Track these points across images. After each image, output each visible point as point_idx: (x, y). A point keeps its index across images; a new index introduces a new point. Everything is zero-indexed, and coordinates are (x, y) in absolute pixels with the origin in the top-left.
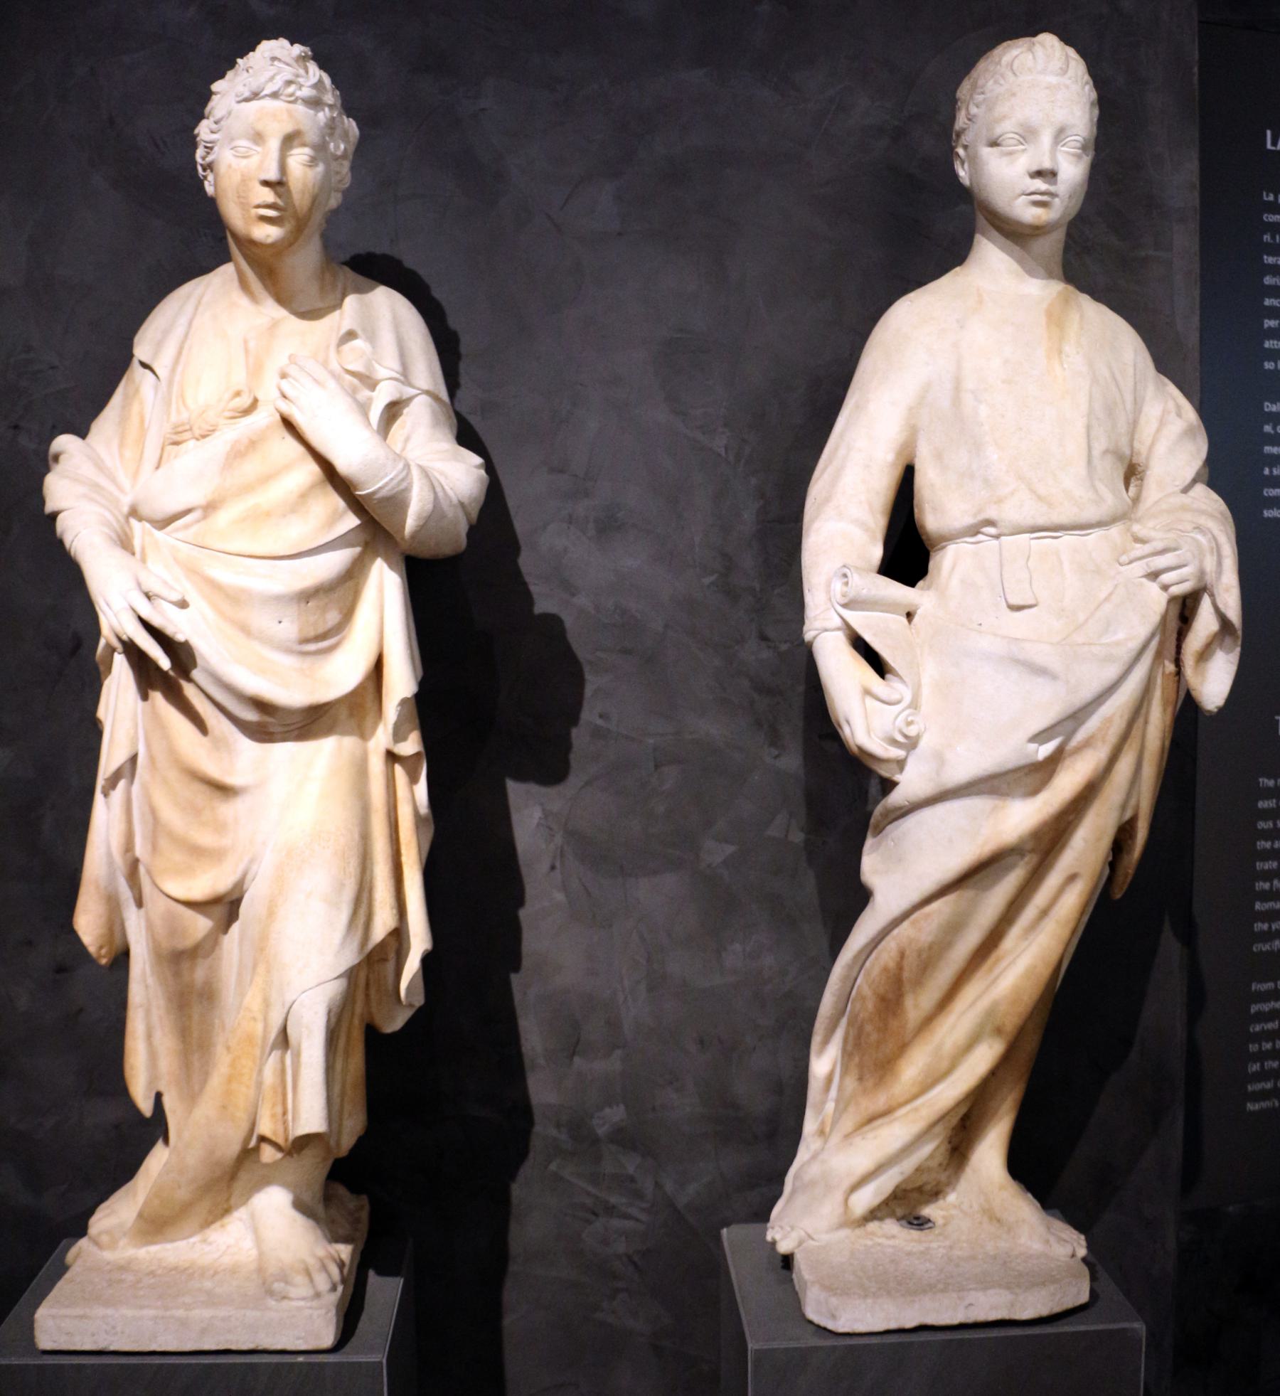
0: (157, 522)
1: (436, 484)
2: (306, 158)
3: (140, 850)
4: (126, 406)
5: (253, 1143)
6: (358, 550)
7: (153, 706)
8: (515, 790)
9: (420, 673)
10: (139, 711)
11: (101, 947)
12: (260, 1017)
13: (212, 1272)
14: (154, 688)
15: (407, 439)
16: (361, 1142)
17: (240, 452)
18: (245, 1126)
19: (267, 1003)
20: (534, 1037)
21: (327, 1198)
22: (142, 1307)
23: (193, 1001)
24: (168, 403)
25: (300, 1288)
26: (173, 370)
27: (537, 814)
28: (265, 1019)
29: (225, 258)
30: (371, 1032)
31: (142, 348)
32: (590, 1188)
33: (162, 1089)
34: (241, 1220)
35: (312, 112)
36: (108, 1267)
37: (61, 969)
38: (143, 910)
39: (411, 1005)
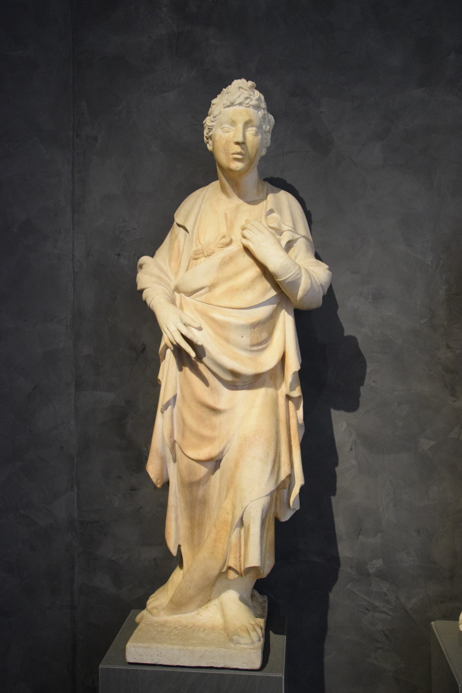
0: (188, 293)
1: (312, 276)
2: (254, 132)
3: (176, 437)
4: (171, 244)
5: (224, 570)
6: (275, 306)
7: (185, 374)
8: (334, 413)
10: (178, 376)
11: (158, 480)
12: (230, 513)
16: (273, 570)
17: (225, 263)
18: (221, 562)
19: (234, 506)
20: (341, 525)
21: (252, 596)
22: (174, 644)
23: (197, 506)
26: (194, 227)
27: (345, 425)
28: (233, 513)
29: (216, 178)
30: (277, 520)
31: (179, 218)
32: (366, 598)
34: (215, 605)
35: (256, 111)
36: (157, 624)
37: (133, 489)
38: (176, 463)
39: (294, 509)
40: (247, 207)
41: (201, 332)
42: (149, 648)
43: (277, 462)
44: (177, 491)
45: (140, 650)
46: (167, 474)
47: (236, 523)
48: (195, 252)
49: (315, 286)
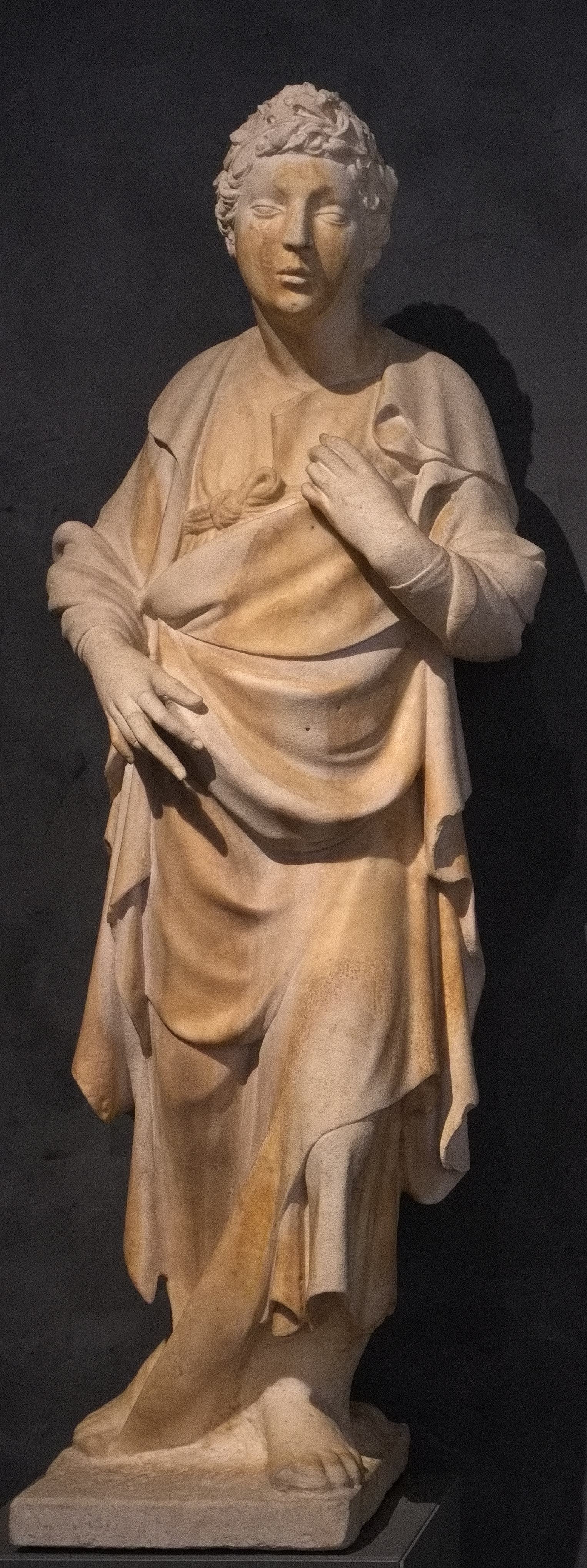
0: (173, 619)
3: (149, 987)
6: (397, 650)
7: (168, 823)
9: (468, 790)
11: (102, 1099)
12: (277, 1167)
13: (217, 1473)
14: (168, 804)
15: (455, 528)
17: (261, 545)
18: (256, 1294)
19: (284, 1150)
21: (355, 1415)
22: (132, 1498)
23: (206, 1167)
24: (186, 488)
25: (310, 1477)
28: (282, 1167)
29: (251, 322)
31: (157, 428)
33: (168, 1273)
34: (250, 1421)
35: (341, 165)
38: (152, 1059)
39: (453, 1171)
40: (328, 398)
41: (202, 716)
42: (68, 1507)
46: (130, 1090)
48: (194, 515)
49: (491, 602)
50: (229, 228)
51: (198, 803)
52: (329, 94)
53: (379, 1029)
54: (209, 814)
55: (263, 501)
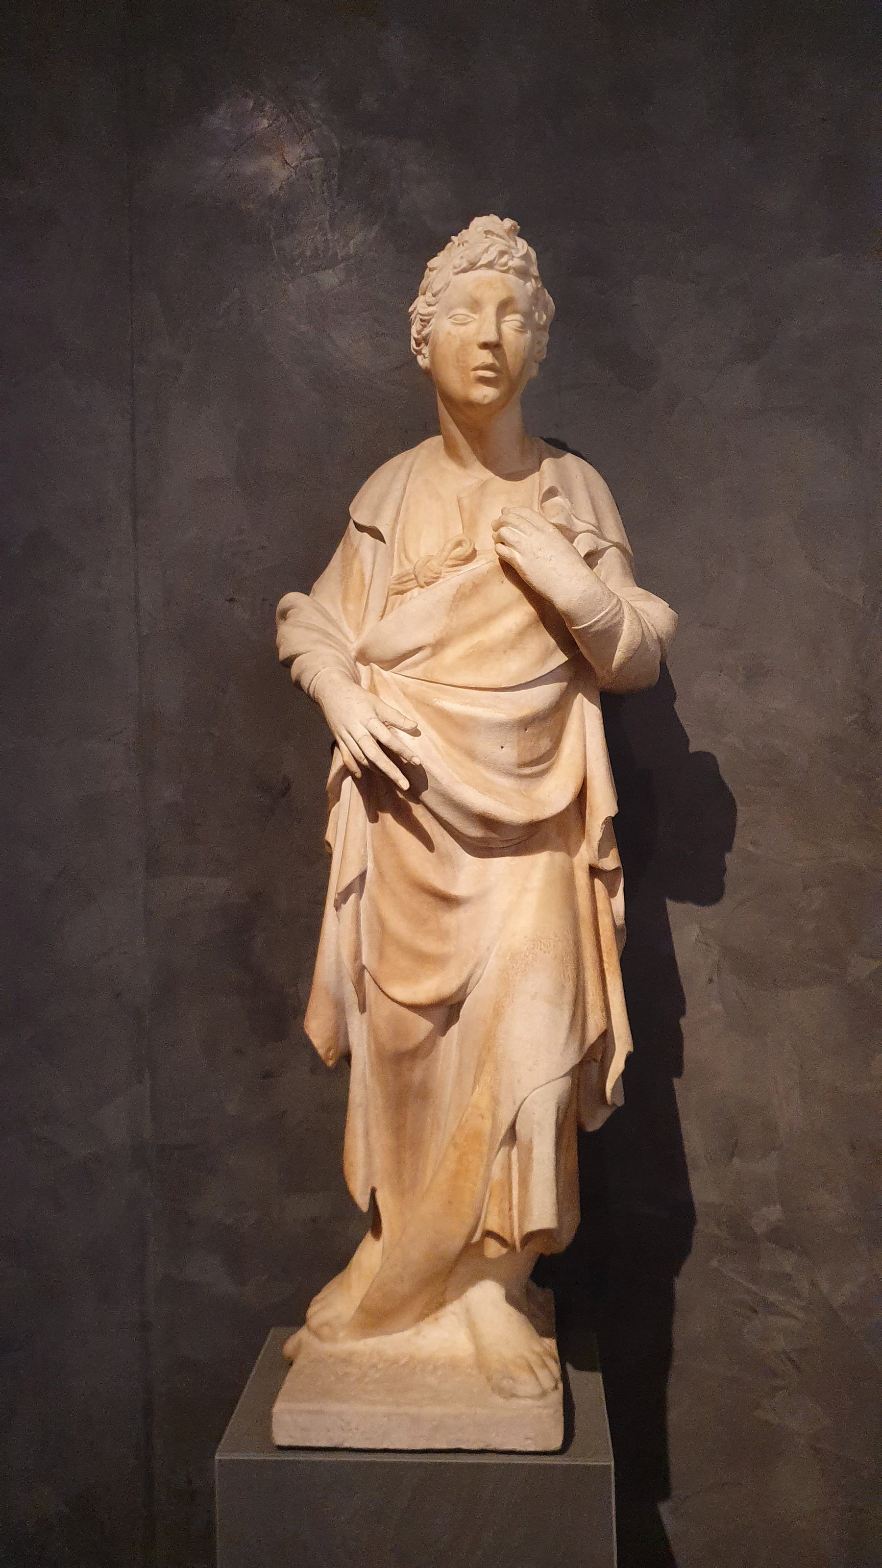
0: (387, 661)
2: (519, 324)
3: (365, 960)
6: (565, 684)
7: (384, 827)
10: (368, 832)
11: (329, 1050)
18: (470, 1221)
19: (495, 1100)
20: (695, 1139)
21: (528, 1293)
26: (393, 529)
31: (361, 511)
33: (377, 1186)
34: (454, 1313)
35: (522, 281)
39: (614, 1104)
40: (499, 483)
43: (581, 1003)
44: (367, 1072)
45: (300, 1419)
47: (501, 1138)
50: (423, 344)
51: (410, 810)
52: (513, 222)
53: (568, 997)
54: (419, 819)
55: (460, 562)
